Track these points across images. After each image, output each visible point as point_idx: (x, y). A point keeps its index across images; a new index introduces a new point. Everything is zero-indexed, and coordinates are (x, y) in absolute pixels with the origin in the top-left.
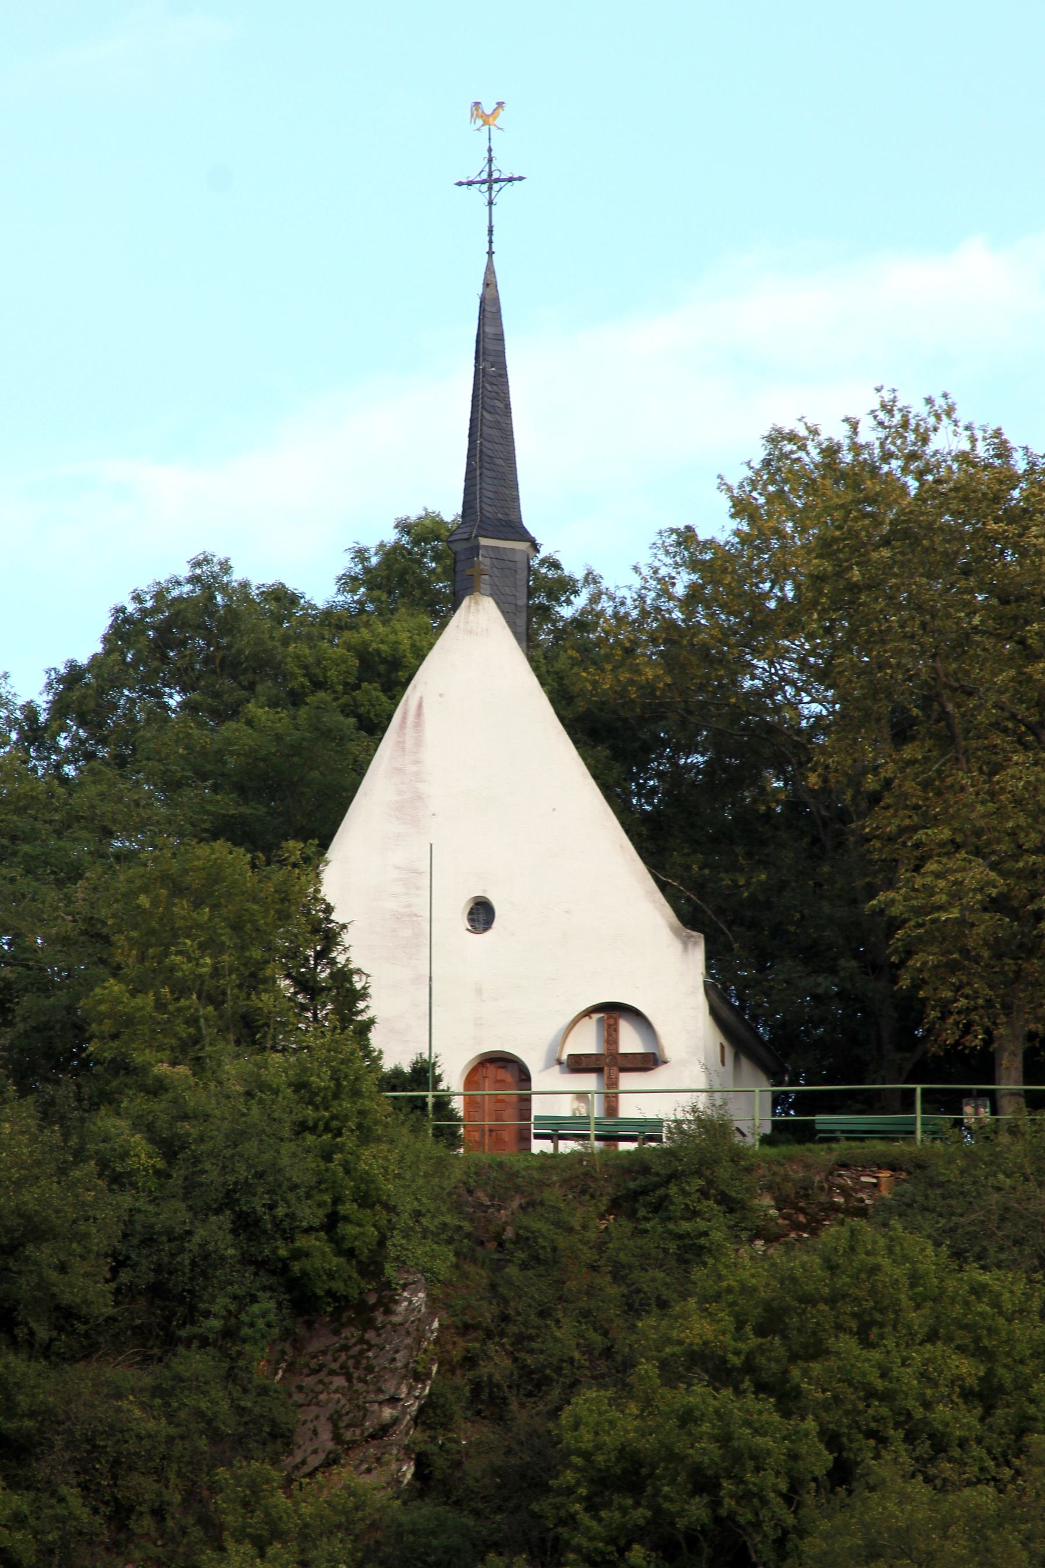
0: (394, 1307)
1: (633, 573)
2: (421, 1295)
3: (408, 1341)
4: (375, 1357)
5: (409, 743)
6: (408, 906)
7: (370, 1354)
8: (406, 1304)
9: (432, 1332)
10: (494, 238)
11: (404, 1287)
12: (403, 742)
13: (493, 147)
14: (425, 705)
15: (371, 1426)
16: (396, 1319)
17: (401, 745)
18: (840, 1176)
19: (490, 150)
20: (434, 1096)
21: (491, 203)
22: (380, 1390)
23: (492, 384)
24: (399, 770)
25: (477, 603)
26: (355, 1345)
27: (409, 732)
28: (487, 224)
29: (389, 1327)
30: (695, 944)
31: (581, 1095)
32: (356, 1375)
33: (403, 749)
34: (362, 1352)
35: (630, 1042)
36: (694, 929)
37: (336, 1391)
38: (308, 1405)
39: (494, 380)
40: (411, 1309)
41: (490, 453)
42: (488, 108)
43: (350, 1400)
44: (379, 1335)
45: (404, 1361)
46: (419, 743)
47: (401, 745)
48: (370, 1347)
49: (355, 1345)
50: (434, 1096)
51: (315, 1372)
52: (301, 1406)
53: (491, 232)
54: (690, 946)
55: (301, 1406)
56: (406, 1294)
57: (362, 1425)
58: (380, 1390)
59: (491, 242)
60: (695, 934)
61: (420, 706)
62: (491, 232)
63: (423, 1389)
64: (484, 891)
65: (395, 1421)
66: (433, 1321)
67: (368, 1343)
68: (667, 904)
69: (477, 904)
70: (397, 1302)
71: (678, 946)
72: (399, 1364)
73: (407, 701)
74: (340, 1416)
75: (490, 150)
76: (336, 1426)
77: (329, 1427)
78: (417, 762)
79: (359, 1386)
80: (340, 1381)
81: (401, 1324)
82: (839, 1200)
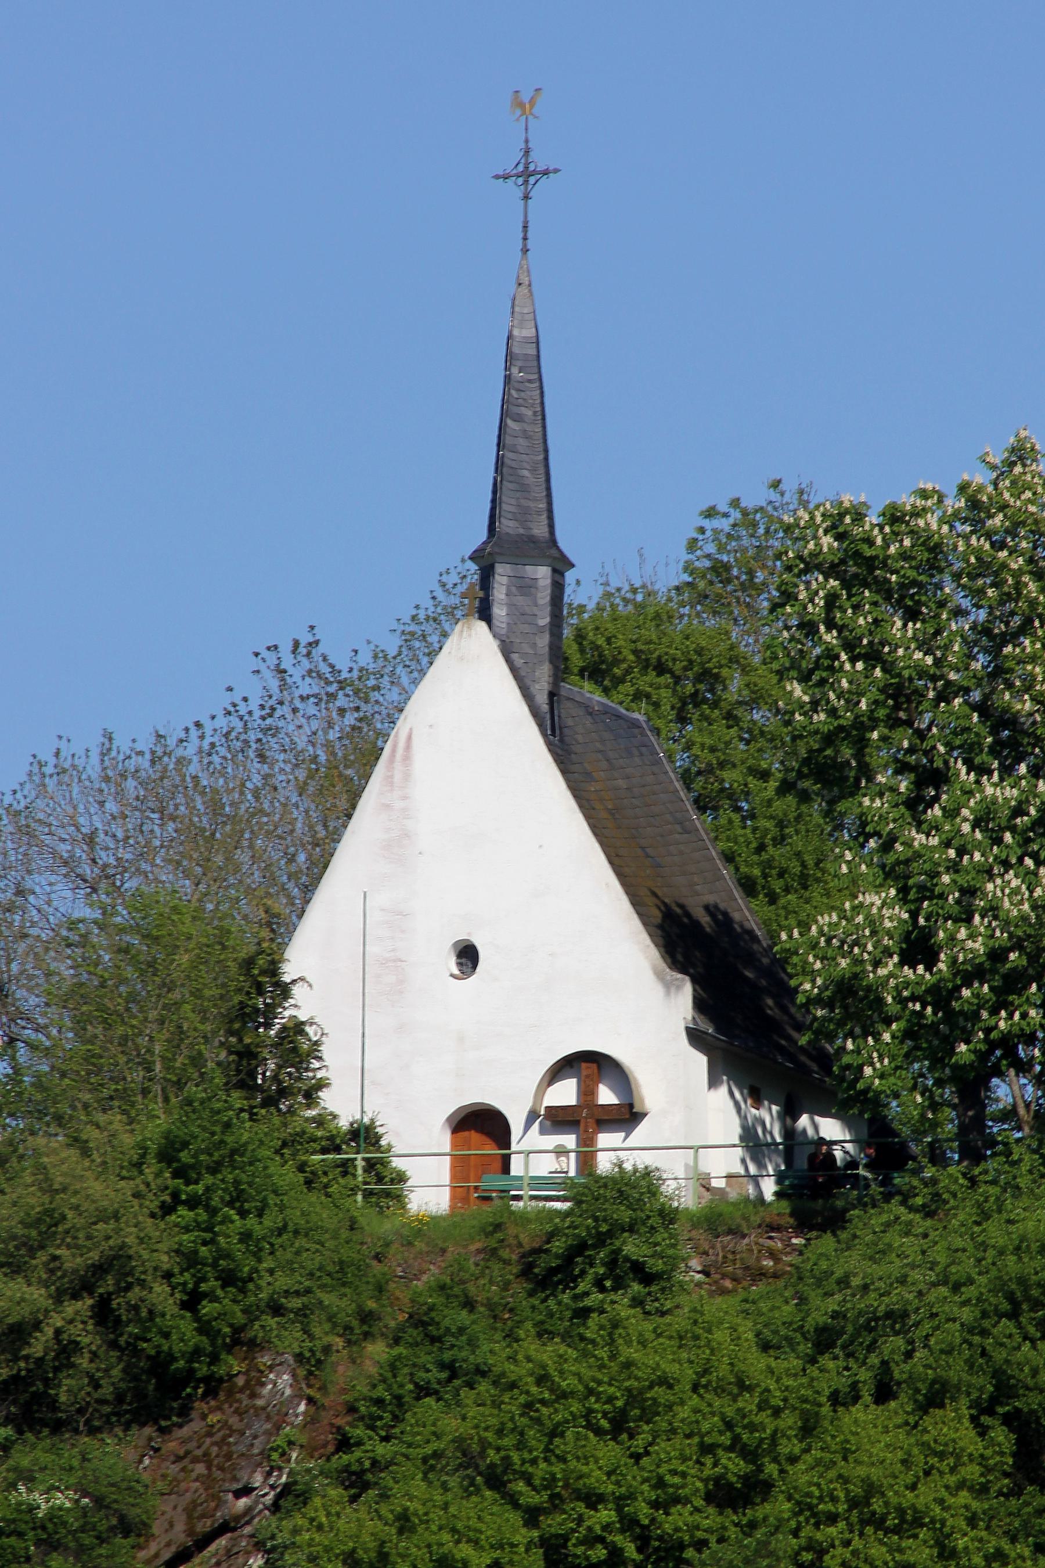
0: (258, 1389)
1: (291, 644)
2: (285, 1377)
3: (268, 1426)
4: (236, 1444)
5: (398, 776)
6: (393, 950)
7: (231, 1440)
8: (270, 1386)
9: (297, 1416)
10: (529, 235)
11: (271, 1368)
12: (392, 777)
13: (530, 138)
14: (414, 737)
15: (222, 1516)
16: (260, 1402)
17: (389, 780)
18: (770, 1238)
19: (527, 141)
20: (364, 1159)
21: (526, 197)
22: (235, 1479)
23: (518, 390)
24: (387, 807)
25: (469, 628)
26: (219, 1430)
27: (398, 765)
28: (522, 218)
29: (252, 1411)
30: (679, 988)
31: (560, 1152)
32: (215, 1462)
33: (392, 784)
34: (224, 1439)
35: (606, 1096)
36: (684, 971)
37: (196, 1480)
38: (169, 1494)
39: (521, 386)
40: (274, 1393)
41: (514, 464)
42: (525, 97)
43: (206, 1490)
44: (241, 1421)
45: (261, 1447)
46: (407, 777)
47: (389, 780)
48: (232, 1432)
49: (219, 1430)
50: (364, 1159)
51: (179, 1459)
52: (163, 1494)
53: (525, 227)
54: (673, 990)
55: (163, 1494)
56: (271, 1376)
57: (213, 1516)
58: (235, 1479)
59: (525, 239)
60: (680, 976)
61: (409, 738)
62: (525, 227)
63: (280, 1477)
64: (469, 934)
65: (249, 1510)
66: (298, 1405)
67: (230, 1428)
68: (652, 946)
69: (466, 947)
70: (263, 1385)
71: (658, 989)
72: (256, 1451)
73: (396, 736)
74: (195, 1507)
75: (527, 141)
76: (190, 1517)
77: (184, 1517)
78: (405, 798)
79: (217, 1474)
80: (200, 1469)
81: (264, 1408)
82: (768, 1263)
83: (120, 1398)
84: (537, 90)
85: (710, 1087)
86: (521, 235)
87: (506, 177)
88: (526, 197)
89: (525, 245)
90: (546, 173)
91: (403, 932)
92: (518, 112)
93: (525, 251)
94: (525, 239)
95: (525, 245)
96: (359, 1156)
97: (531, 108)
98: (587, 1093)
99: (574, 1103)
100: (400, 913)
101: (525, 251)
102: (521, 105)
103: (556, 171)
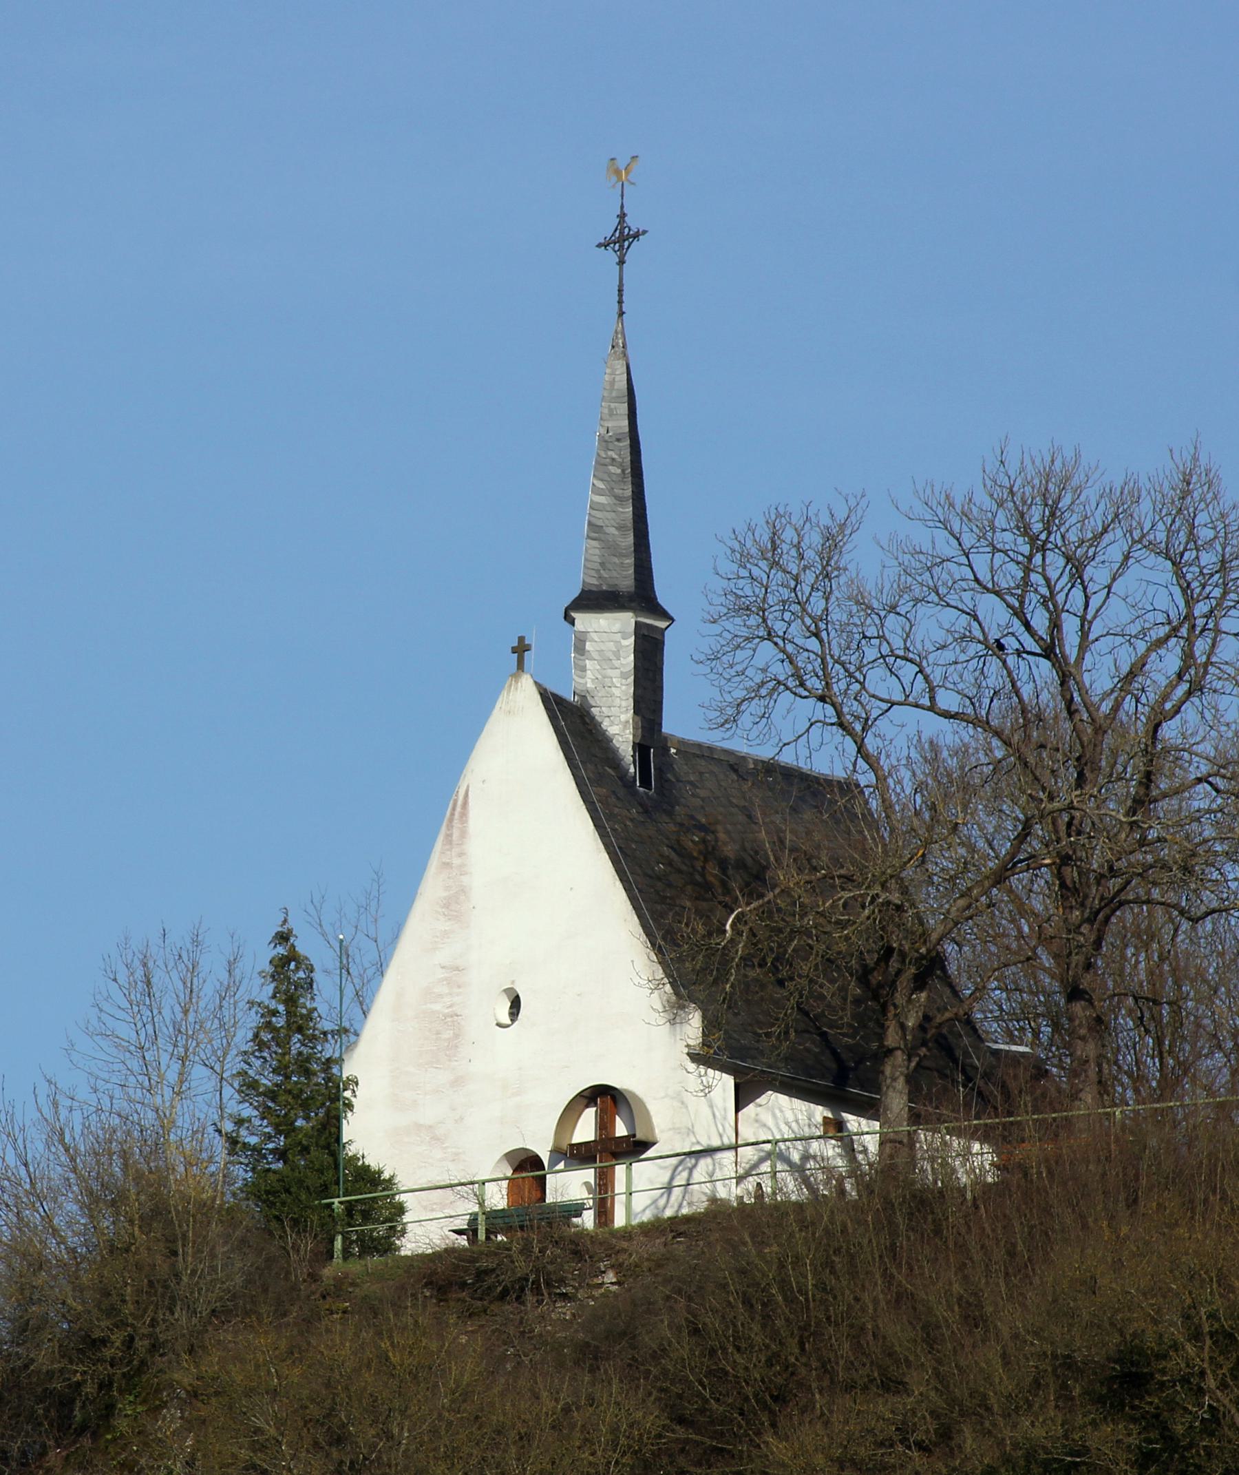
5: (456, 834)
6: (451, 1006)
19: (622, 207)
21: (621, 262)
24: (447, 865)
25: (517, 682)
27: (456, 823)
42: (621, 164)
46: (464, 834)
53: (620, 291)
59: (620, 302)
62: (620, 291)
64: (513, 982)
75: (622, 207)
78: (461, 855)
83: (923, 957)
84: (634, 157)
85: (654, 1144)
86: (617, 299)
87: (606, 246)
88: (621, 262)
89: (621, 308)
90: (636, 236)
91: (459, 987)
92: (614, 178)
93: (621, 313)
94: (620, 302)
95: (621, 308)
96: (336, 1201)
97: (627, 174)
98: (604, 1125)
99: (593, 1139)
100: (457, 969)
101: (621, 313)
102: (617, 172)
103: (645, 232)
